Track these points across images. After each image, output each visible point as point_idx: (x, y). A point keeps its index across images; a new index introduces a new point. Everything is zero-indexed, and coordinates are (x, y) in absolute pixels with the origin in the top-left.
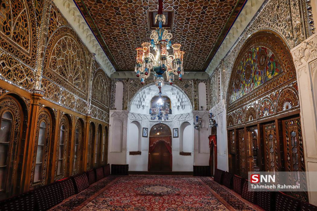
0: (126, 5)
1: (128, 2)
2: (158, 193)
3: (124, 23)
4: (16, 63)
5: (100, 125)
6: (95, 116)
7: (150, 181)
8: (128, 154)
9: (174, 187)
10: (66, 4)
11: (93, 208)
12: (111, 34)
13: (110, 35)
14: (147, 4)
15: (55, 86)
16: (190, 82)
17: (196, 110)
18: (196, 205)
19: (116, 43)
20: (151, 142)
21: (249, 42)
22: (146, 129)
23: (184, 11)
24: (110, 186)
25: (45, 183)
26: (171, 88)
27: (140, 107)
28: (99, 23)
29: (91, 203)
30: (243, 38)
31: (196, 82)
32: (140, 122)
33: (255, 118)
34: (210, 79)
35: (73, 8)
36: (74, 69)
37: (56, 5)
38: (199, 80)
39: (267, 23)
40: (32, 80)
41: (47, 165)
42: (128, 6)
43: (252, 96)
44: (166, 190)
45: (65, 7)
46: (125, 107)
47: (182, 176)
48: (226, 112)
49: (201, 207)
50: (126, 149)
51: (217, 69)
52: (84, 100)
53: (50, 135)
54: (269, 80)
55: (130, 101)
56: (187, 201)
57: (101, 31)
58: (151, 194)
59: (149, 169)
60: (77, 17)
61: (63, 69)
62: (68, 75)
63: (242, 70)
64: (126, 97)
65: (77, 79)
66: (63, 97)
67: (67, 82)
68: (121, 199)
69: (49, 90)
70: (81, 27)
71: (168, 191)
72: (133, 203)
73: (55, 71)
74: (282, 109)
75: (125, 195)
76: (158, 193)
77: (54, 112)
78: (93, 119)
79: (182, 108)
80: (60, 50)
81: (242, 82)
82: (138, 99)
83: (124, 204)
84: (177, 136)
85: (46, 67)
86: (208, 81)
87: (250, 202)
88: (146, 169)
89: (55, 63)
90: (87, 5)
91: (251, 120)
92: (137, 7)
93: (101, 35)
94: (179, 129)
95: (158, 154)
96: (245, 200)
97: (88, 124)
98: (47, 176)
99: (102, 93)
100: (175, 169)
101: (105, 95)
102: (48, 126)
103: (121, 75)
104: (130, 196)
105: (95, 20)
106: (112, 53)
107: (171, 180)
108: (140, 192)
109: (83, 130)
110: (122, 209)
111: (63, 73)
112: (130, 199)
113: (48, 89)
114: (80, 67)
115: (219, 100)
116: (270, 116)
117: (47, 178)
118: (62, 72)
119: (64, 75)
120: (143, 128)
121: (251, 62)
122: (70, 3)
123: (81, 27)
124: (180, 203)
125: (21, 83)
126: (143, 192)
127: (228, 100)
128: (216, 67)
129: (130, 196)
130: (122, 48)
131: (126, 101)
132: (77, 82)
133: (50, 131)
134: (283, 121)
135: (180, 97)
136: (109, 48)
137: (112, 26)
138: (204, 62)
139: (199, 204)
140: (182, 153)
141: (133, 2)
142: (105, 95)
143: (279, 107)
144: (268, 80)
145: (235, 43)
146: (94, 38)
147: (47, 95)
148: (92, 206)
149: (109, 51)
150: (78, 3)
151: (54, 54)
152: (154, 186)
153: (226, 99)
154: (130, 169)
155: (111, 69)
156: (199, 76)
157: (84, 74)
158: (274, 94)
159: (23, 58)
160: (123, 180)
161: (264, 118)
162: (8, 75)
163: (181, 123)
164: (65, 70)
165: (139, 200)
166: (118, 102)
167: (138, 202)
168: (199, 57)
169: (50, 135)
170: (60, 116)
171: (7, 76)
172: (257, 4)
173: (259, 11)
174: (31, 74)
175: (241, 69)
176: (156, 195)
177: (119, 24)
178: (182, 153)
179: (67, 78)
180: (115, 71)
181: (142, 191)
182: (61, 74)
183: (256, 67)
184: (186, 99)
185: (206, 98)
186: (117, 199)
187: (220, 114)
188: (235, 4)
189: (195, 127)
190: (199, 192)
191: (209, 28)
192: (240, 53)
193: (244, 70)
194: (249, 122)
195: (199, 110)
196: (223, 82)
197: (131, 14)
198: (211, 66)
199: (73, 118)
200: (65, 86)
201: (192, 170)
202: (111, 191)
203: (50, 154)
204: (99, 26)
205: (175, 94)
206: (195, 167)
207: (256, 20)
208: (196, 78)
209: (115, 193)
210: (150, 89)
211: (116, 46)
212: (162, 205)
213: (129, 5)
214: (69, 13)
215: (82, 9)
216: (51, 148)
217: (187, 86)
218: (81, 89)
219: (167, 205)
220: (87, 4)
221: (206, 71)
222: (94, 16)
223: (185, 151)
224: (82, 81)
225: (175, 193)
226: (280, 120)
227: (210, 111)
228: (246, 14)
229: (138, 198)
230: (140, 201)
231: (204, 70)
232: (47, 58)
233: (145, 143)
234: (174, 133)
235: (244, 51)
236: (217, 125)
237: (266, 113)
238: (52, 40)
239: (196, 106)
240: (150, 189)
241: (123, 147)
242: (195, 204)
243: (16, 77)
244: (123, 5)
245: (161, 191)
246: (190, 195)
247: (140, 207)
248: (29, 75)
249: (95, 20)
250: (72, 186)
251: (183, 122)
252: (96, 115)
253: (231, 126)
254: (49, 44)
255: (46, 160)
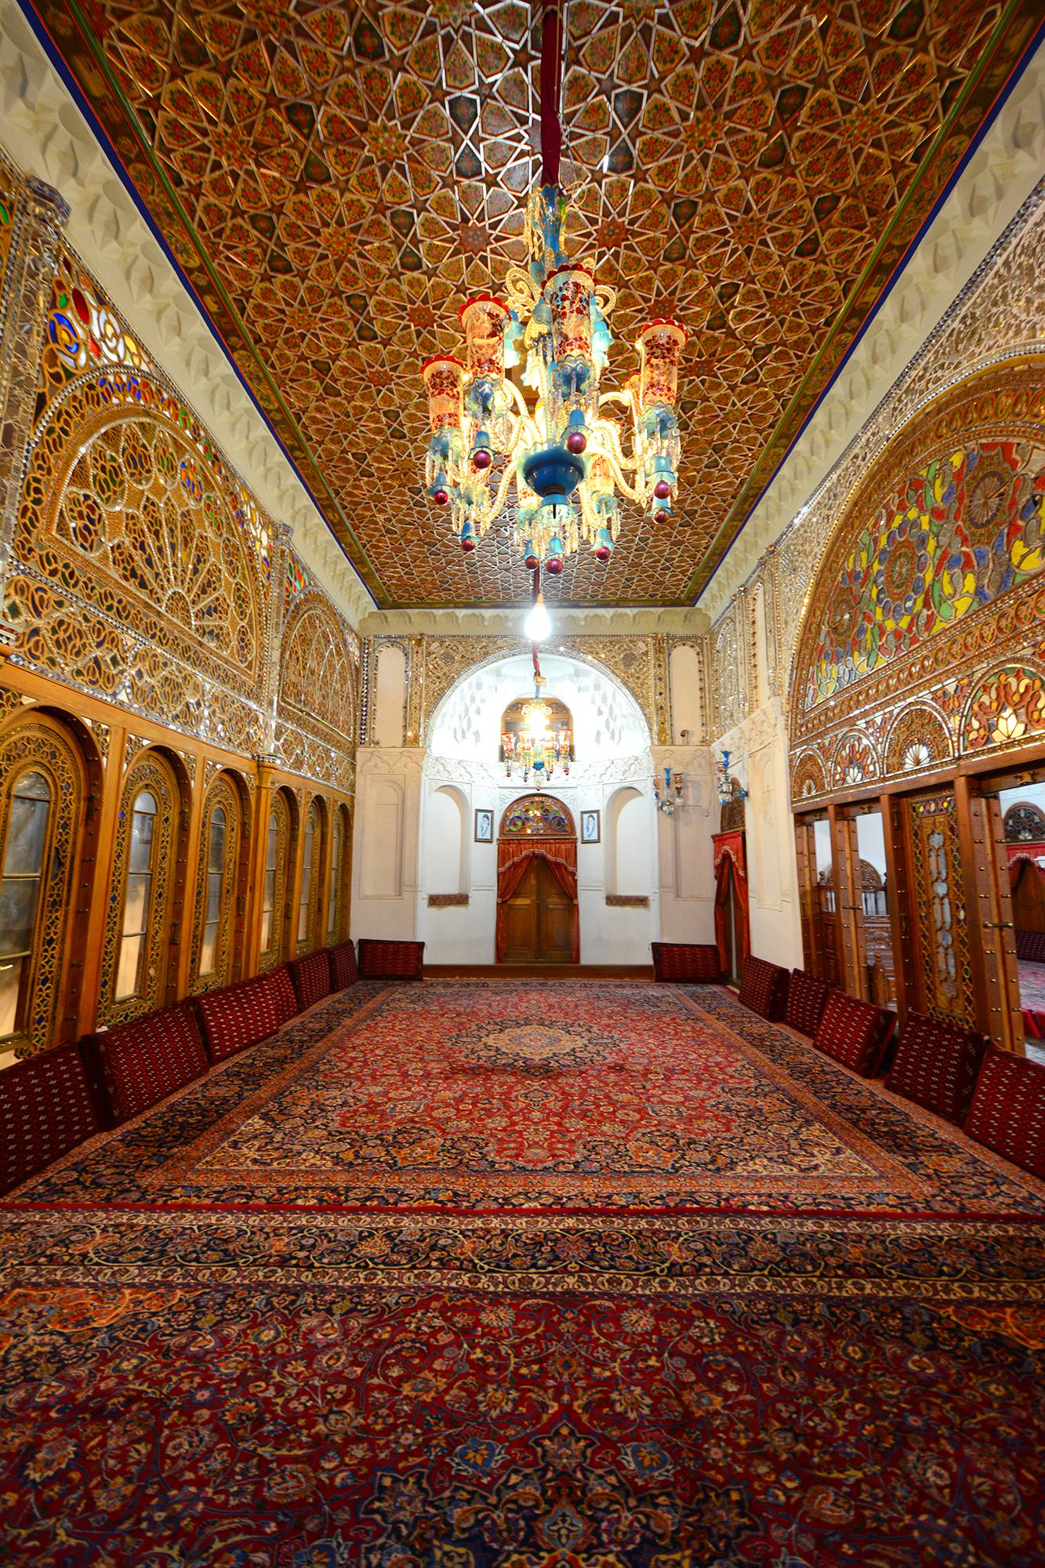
0: (394, 280)
1: (403, 266)
2: (537, 1058)
3: (393, 386)
4: (165, 664)
5: (319, 801)
6: (298, 764)
7: (503, 1004)
8: (423, 903)
9: (595, 1029)
10: (136, 276)
11: (259, 1150)
12: (346, 437)
13: (340, 442)
14: (483, 275)
15: (94, 620)
16: (640, 644)
17: (662, 743)
18: (705, 1127)
19: (367, 484)
20: (502, 857)
21: (904, 448)
22: (488, 813)
23: (640, 316)
24: (353, 1032)
25: (50, 1042)
26: (572, 671)
27: (464, 737)
28: (292, 381)
29: (256, 1122)
30: (874, 434)
31: (663, 645)
32: (465, 789)
33: (820, 786)
34: (712, 634)
35: (174, 298)
36: (196, 571)
37: (84, 262)
38: (674, 637)
39: (1018, 326)
40: (114, 661)
41: (61, 959)
42: (405, 288)
43: (923, 666)
44: (567, 1044)
45: (217, 408)
46: (413, 738)
47: (618, 982)
48: (787, 743)
49: (728, 1135)
50: (414, 886)
51: (745, 590)
52: (248, 697)
53: (75, 833)
54: (1025, 582)
55: (429, 714)
56: (663, 1102)
57: (305, 427)
58: (510, 1069)
59: (499, 955)
60: (223, 385)
61: (138, 556)
62: (162, 588)
63: (869, 567)
64: (416, 701)
65: (210, 611)
66: (140, 674)
67: (159, 614)
68: (386, 1094)
69: (62, 635)
70: (287, 499)
71: (573, 1050)
72: (435, 1114)
73: (92, 556)
74: (902, 765)
75: (405, 1075)
76: (537, 1058)
77: (94, 736)
78: (284, 772)
79: (613, 737)
80: (116, 471)
81: (868, 618)
82: (460, 709)
83: (399, 1123)
84: (594, 837)
85: (34, 527)
86: (703, 642)
87: (937, 1110)
88: (486, 956)
89: (92, 522)
90: (230, 283)
91: (809, 792)
92: (442, 291)
93: (307, 444)
94: (602, 814)
95: (527, 901)
96: (912, 1105)
97: (264, 792)
98: (60, 1010)
99: (326, 684)
100: (589, 956)
101: (336, 692)
102: (61, 793)
103: (397, 622)
104: (428, 1075)
105: (273, 366)
106: (356, 528)
107: (575, 993)
108: (467, 1056)
109: (244, 814)
110: (388, 1153)
111: (134, 574)
112: (425, 1096)
113: (84, 645)
114: (223, 567)
115: (752, 702)
116: (932, 767)
117: (60, 1018)
118: (133, 570)
119: (143, 585)
120: (478, 811)
121: (915, 523)
122: (119, 211)
123: (287, 499)
124: (638, 1116)
125: (79, 673)
126: (479, 1058)
127: (797, 695)
128: (743, 581)
129: (428, 1075)
130: (392, 508)
131: (415, 715)
132: (210, 622)
133: (73, 816)
134: (905, 801)
135: (604, 700)
136: (344, 508)
137: (346, 398)
138: (697, 564)
139: (716, 1116)
140: (613, 900)
141: (425, 268)
142: (336, 692)
143: (893, 760)
144: (1019, 579)
145: (816, 490)
146: (279, 456)
147: (47, 654)
148: (255, 1137)
149: (344, 517)
150: (190, 271)
151: (79, 477)
152: (518, 1025)
153: (786, 695)
154: (429, 958)
155: (344, 575)
156: (673, 621)
157: (241, 599)
158: (951, 688)
159: (50, 564)
160: (401, 998)
161: (994, 749)
162: (31, 644)
163: (610, 790)
164: (149, 562)
165: (460, 1100)
166: (387, 721)
167: (458, 1111)
168: (681, 543)
169: (75, 833)
170: (125, 757)
171: (26, 648)
172: (960, 257)
173: (1000, 244)
174: (113, 640)
175: (864, 565)
176: (529, 1070)
177: (373, 389)
178: (613, 900)
179: (159, 600)
180: (374, 608)
181: (473, 1052)
182: (126, 578)
183: (944, 540)
184: (625, 704)
185: (698, 703)
186: (370, 1095)
187: (759, 755)
188: (859, 266)
189: (660, 808)
190: (700, 1056)
191: (734, 404)
192: (856, 504)
193: (876, 567)
194: (907, 774)
195: (673, 744)
196: (773, 633)
197: (419, 334)
198: (719, 583)
199: (198, 767)
200: (152, 631)
201: (647, 959)
202: (353, 1055)
203: (78, 912)
204: (292, 399)
205: (587, 689)
206: (657, 948)
207: (951, 335)
208: (662, 630)
209: (365, 1062)
210: (498, 673)
211: (371, 498)
212: (559, 1124)
213: (411, 284)
214: (158, 320)
215: (209, 301)
216: (81, 886)
217: (629, 659)
218: (232, 654)
219: (581, 1124)
220: (231, 277)
221: (699, 605)
222: (268, 344)
223: (623, 891)
224: (233, 624)
225: (605, 1058)
226: (897, 797)
227: (716, 747)
228: (875, 359)
229: (460, 1086)
230: (466, 1106)
231: (693, 599)
232: (42, 487)
233: (485, 864)
234: (585, 828)
235: (879, 487)
236: (747, 794)
237: (854, 775)
238: (67, 413)
239: (662, 731)
240: (504, 1042)
241: (407, 879)
242: (698, 1118)
243: (62, 651)
244: (385, 281)
245: (547, 1053)
246: (667, 1069)
247: (465, 1138)
248: (106, 645)
249: (273, 366)
250: (78, 1091)
251: (618, 787)
252: (302, 763)
253: (813, 793)
254: (50, 431)
255: (51, 941)
